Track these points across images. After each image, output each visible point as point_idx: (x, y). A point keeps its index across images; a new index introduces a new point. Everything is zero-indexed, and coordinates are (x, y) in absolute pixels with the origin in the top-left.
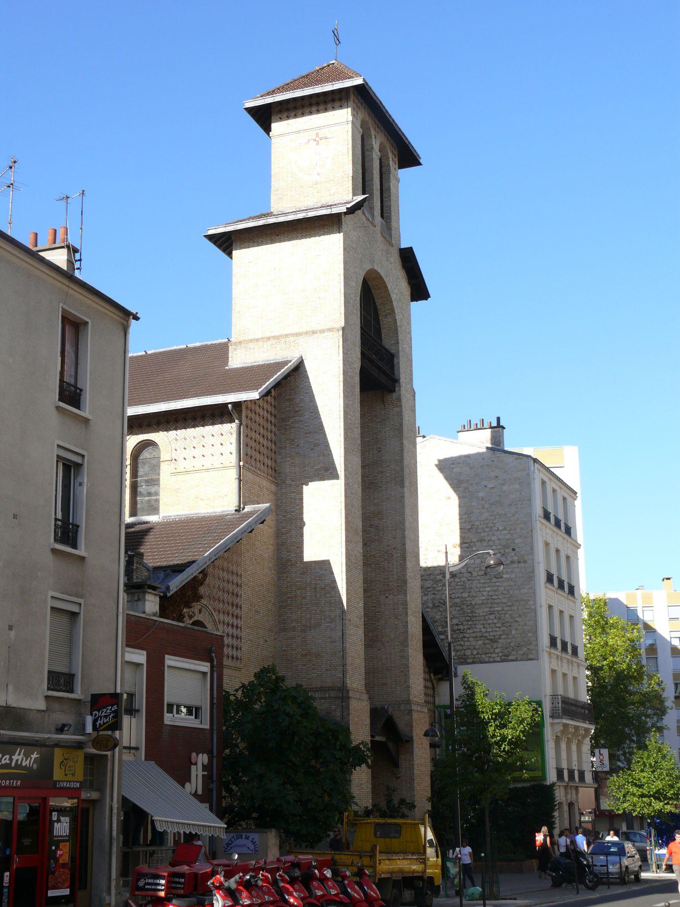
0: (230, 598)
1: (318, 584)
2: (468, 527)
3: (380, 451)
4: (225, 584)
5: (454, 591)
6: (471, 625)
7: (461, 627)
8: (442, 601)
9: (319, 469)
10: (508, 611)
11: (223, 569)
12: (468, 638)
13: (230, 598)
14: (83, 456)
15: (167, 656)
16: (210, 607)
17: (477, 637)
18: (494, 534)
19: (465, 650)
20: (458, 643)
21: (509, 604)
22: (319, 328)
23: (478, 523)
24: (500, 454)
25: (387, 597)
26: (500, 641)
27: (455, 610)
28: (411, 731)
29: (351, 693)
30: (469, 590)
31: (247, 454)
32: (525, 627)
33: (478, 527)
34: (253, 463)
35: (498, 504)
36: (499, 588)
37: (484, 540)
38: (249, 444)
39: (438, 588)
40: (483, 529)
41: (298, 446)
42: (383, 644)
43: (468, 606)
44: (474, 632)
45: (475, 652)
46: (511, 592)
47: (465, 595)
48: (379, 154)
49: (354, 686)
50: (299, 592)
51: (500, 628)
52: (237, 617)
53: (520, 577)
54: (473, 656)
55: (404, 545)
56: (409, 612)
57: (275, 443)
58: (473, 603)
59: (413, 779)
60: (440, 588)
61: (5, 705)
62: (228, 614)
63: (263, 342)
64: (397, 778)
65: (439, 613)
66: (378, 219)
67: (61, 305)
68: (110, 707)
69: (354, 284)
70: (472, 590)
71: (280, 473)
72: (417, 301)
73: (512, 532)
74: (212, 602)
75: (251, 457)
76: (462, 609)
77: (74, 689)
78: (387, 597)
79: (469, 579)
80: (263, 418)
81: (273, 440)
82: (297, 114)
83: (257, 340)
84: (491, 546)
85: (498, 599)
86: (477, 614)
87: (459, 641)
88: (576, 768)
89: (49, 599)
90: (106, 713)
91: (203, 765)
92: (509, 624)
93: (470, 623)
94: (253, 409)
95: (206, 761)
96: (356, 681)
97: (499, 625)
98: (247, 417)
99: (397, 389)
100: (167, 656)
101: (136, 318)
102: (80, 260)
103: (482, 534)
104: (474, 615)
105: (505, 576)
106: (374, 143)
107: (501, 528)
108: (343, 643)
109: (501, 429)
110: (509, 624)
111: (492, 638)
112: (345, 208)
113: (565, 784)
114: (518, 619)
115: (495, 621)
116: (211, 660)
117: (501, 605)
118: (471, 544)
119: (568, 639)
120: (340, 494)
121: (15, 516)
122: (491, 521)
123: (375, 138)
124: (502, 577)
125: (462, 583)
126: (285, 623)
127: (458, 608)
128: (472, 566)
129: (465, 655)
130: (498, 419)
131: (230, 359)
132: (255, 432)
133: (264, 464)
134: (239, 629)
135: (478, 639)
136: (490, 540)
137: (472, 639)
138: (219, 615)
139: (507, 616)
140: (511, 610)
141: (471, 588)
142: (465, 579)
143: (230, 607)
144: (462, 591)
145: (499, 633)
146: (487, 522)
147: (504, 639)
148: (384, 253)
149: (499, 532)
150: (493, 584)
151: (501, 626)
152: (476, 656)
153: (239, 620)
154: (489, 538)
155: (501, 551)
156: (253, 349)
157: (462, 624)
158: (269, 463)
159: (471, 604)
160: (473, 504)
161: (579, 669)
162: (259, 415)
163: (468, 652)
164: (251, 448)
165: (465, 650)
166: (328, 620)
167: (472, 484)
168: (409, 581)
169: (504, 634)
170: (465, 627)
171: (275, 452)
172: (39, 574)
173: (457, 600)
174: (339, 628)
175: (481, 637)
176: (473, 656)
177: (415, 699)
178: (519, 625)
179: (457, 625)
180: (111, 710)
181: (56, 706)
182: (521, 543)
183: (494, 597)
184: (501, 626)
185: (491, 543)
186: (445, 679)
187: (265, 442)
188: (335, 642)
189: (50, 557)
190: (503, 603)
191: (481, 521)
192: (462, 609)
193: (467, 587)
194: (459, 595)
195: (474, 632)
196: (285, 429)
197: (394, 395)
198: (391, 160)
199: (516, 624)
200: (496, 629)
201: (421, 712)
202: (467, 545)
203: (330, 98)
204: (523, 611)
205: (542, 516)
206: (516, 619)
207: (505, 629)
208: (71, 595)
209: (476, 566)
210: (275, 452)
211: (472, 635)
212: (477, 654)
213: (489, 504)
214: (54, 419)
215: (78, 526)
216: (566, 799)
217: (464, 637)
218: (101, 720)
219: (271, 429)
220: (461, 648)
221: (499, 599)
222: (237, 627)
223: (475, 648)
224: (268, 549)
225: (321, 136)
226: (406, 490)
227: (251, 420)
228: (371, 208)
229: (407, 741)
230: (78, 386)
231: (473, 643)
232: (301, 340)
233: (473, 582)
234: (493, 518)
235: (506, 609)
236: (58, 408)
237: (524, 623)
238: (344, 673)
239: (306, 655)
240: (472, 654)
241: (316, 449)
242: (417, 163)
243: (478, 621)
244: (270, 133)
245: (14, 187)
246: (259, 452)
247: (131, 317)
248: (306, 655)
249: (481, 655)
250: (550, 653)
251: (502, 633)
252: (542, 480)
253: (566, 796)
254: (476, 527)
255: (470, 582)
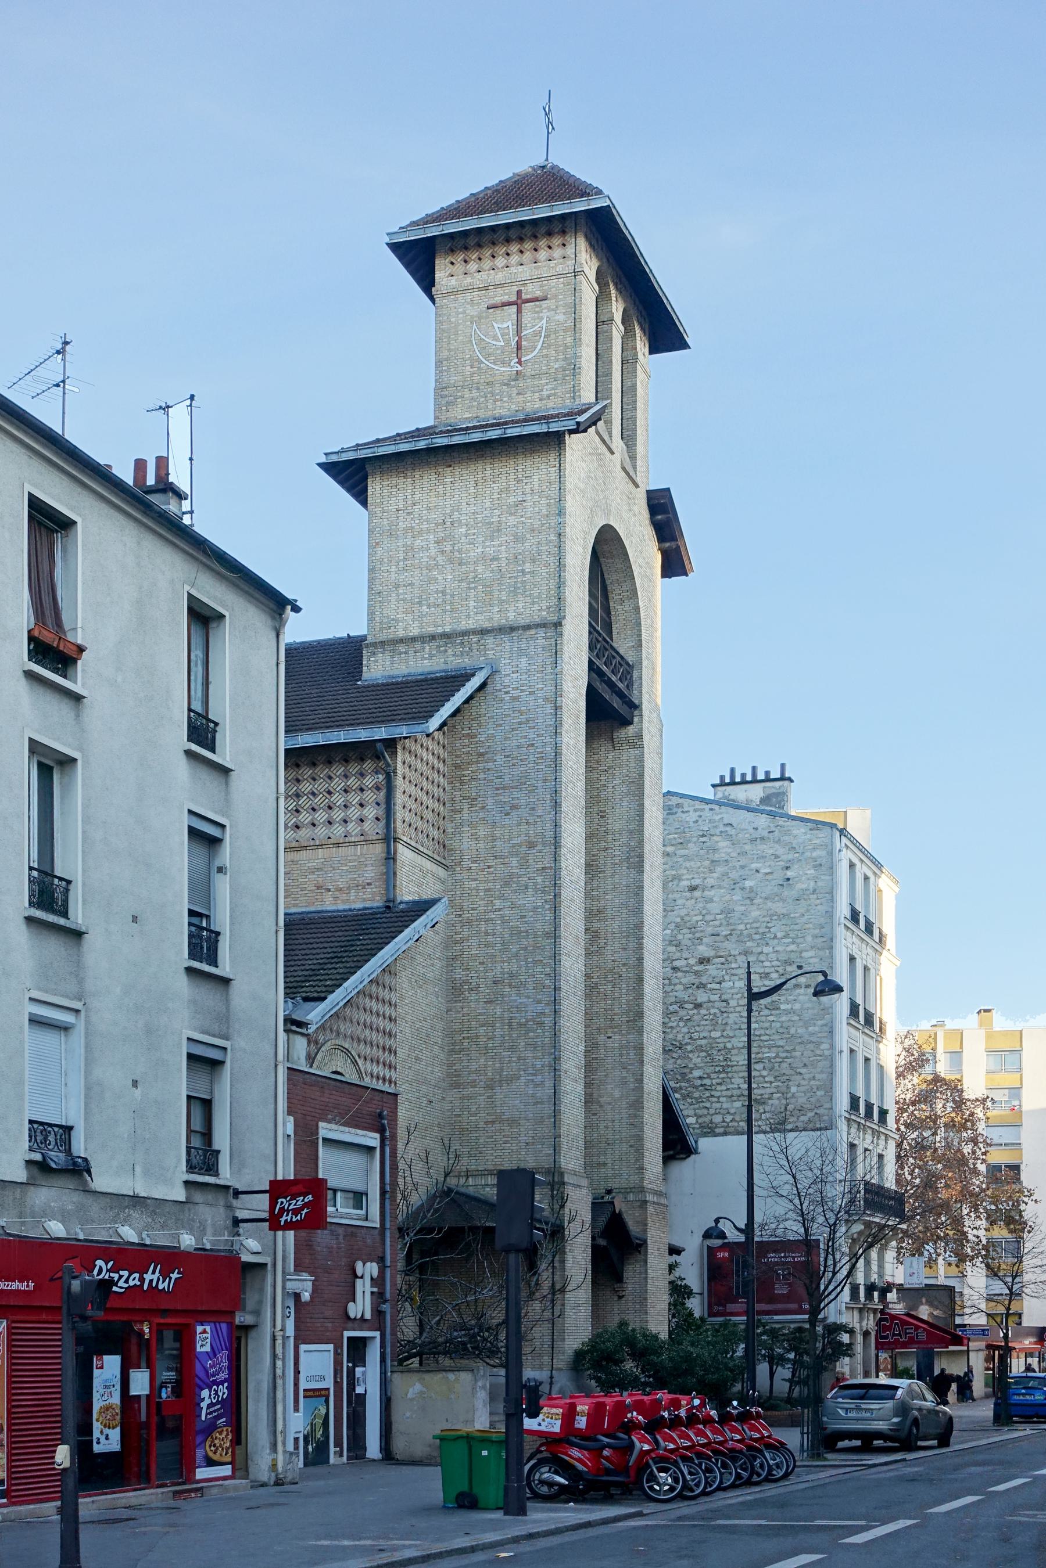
0: (381, 1040)
1: (516, 1018)
2: (724, 933)
3: (604, 816)
4: (374, 1019)
5: (697, 1028)
6: (723, 1078)
7: (707, 1082)
8: (678, 1044)
9: (520, 845)
10: (787, 1057)
11: (371, 997)
12: (718, 1097)
13: (381, 1040)
14: (223, 826)
15: (321, 1124)
16: (353, 1052)
17: (732, 1096)
18: (767, 944)
19: (712, 1115)
20: (703, 1104)
21: (787, 1048)
22: (521, 622)
23: (742, 927)
24: (784, 821)
25: (609, 1037)
26: (770, 1102)
27: (698, 1057)
28: (645, 1231)
29: (566, 1176)
30: (722, 1028)
31: (404, 821)
32: (812, 1082)
33: (741, 934)
34: (413, 834)
35: (776, 899)
36: (773, 1024)
37: (752, 952)
38: (407, 806)
39: (671, 1024)
40: (750, 935)
41: (483, 808)
42: (601, 1106)
43: (719, 1050)
44: (728, 1089)
45: (728, 1118)
46: (792, 1031)
47: (716, 1034)
48: (622, 328)
49: (570, 1166)
50: (482, 1030)
51: (771, 1083)
52: (390, 1067)
53: (808, 1009)
54: (725, 1124)
55: (640, 959)
56: (646, 1060)
57: (444, 804)
58: (729, 1045)
59: (646, 1299)
60: (674, 1024)
61: (132, 1194)
62: (378, 1062)
63: (423, 642)
64: (620, 1297)
65: (672, 1061)
66: (617, 444)
67: (187, 588)
68: (302, 1198)
69: (581, 549)
70: (728, 1028)
71: (452, 850)
72: (670, 577)
73: (799, 940)
74: (355, 1045)
75: (410, 825)
76: (709, 1055)
77: (220, 1171)
78: (609, 1037)
79: (724, 1010)
80: (427, 764)
81: (442, 799)
82: (482, 257)
83: (414, 639)
84: (762, 962)
85: (770, 1040)
86: (735, 1063)
87: (703, 1102)
88: (863, 1283)
89: (185, 1042)
90: (295, 1205)
91: (372, 1278)
92: (785, 1077)
93: (722, 1075)
94: (413, 750)
95: (375, 1274)
96: (571, 1160)
97: (771, 1079)
98: (404, 763)
99: (636, 719)
100: (321, 1124)
101: (296, 609)
102: (191, 512)
103: (749, 944)
104: (729, 1063)
105: (783, 1007)
106: (614, 310)
107: (779, 935)
108: (555, 1104)
109: (786, 783)
110: (785, 1077)
111: (759, 1097)
112: (573, 422)
113: (862, 1306)
114: (803, 1071)
115: (764, 1073)
116: (381, 1130)
117: (774, 1049)
118: (729, 959)
119: (873, 1100)
120: (553, 883)
121: (135, 919)
122: (765, 924)
123: (617, 301)
124: (779, 1009)
125: (711, 1017)
126: (459, 1076)
127: (704, 1054)
128: (728, 991)
129: (711, 1122)
130: (783, 766)
131: (365, 669)
132: (416, 785)
133: (428, 836)
134: (393, 1085)
135: (735, 1098)
136: (761, 953)
137: (725, 1099)
138: (365, 1064)
139: (784, 1065)
140: (791, 1057)
141: (726, 1024)
142: (717, 1011)
143: (381, 1052)
144: (711, 1028)
145: (768, 1091)
146: (758, 925)
147: (778, 1099)
148: (625, 497)
149: (776, 941)
150: (763, 1019)
151: (773, 1080)
152: (730, 1124)
153: (393, 1070)
154: (759, 950)
155: (779, 969)
156: (405, 653)
157: (709, 1077)
158: (435, 833)
159: (725, 1047)
160: (735, 898)
161: (886, 1143)
162: (422, 760)
163: (718, 1119)
164: (410, 810)
165: (712, 1115)
166: (530, 1071)
167: (734, 867)
168: (647, 1013)
169: (778, 1092)
170: (714, 1082)
171: (444, 818)
172: (170, 1005)
173: (703, 1042)
174: (549, 1083)
175: (739, 1096)
176: (725, 1124)
177: (650, 1186)
178: (804, 1079)
179: (700, 1078)
180: (303, 1200)
181: (198, 1196)
182: (811, 957)
183: (762, 1038)
184: (773, 1080)
185: (762, 958)
186: (678, 1157)
187: (430, 803)
188: (542, 1103)
189: (183, 979)
190: (779, 1047)
191: (747, 923)
192: (709, 1055)
193: (720, 1022)
194: (705, 1034)
195: (728, 1089)
196: (461, 782)
197: (631, 730)
198: (638, 338)
199: (798, 1077)
200: (765, 1085)
201: (658, 1204)
202: (722, 960)
203: (543, 230)
204: (811, 1059)
205: (849, 917)
206: (798, 1070)
207: (780, 1084)
208: (214, 1036)
209: (735, 991)
210: (444, 818)
211: (724, 1093)
212: (731, 1121)
213: (761, 897)
214: (182, 768)
215: (218, 934)
216: (861, 1327)
217: (712, 1096)
218: (287, 1215)
219: (438, 782)
220: (705, 1112)
221: (773, 1040)
222: (390, 1082)
223: (728, 1113)
224: (433, 965)
225: (524, 297)
226: (645, 876)
227: (410, 767)
228: (609, 423)
229: (640, 1245)
230: (210, 717)
231: (725, 1106)
232: (490, 640)
233: (730, 1015)
234: (767, 919)
235: (781, 1055)
236: (189, 753)
237: (811, 1075)
238: (556, 1148)
239: (493, 1122)
240: (724, 1121)
241: (514, 813)
242: (683, 345)
243: (735, 1072)
244: (434, 289)
245: (67, 387)
246: (422, 818)
247: (289, 607)
248: (493, 1122)
249: (738, 1122)
250: (848, 1120)
251: (775, 1090)
252: (850, 861)
253: (860, 1323)
254: (739, 932)
255: (725, 1015)
